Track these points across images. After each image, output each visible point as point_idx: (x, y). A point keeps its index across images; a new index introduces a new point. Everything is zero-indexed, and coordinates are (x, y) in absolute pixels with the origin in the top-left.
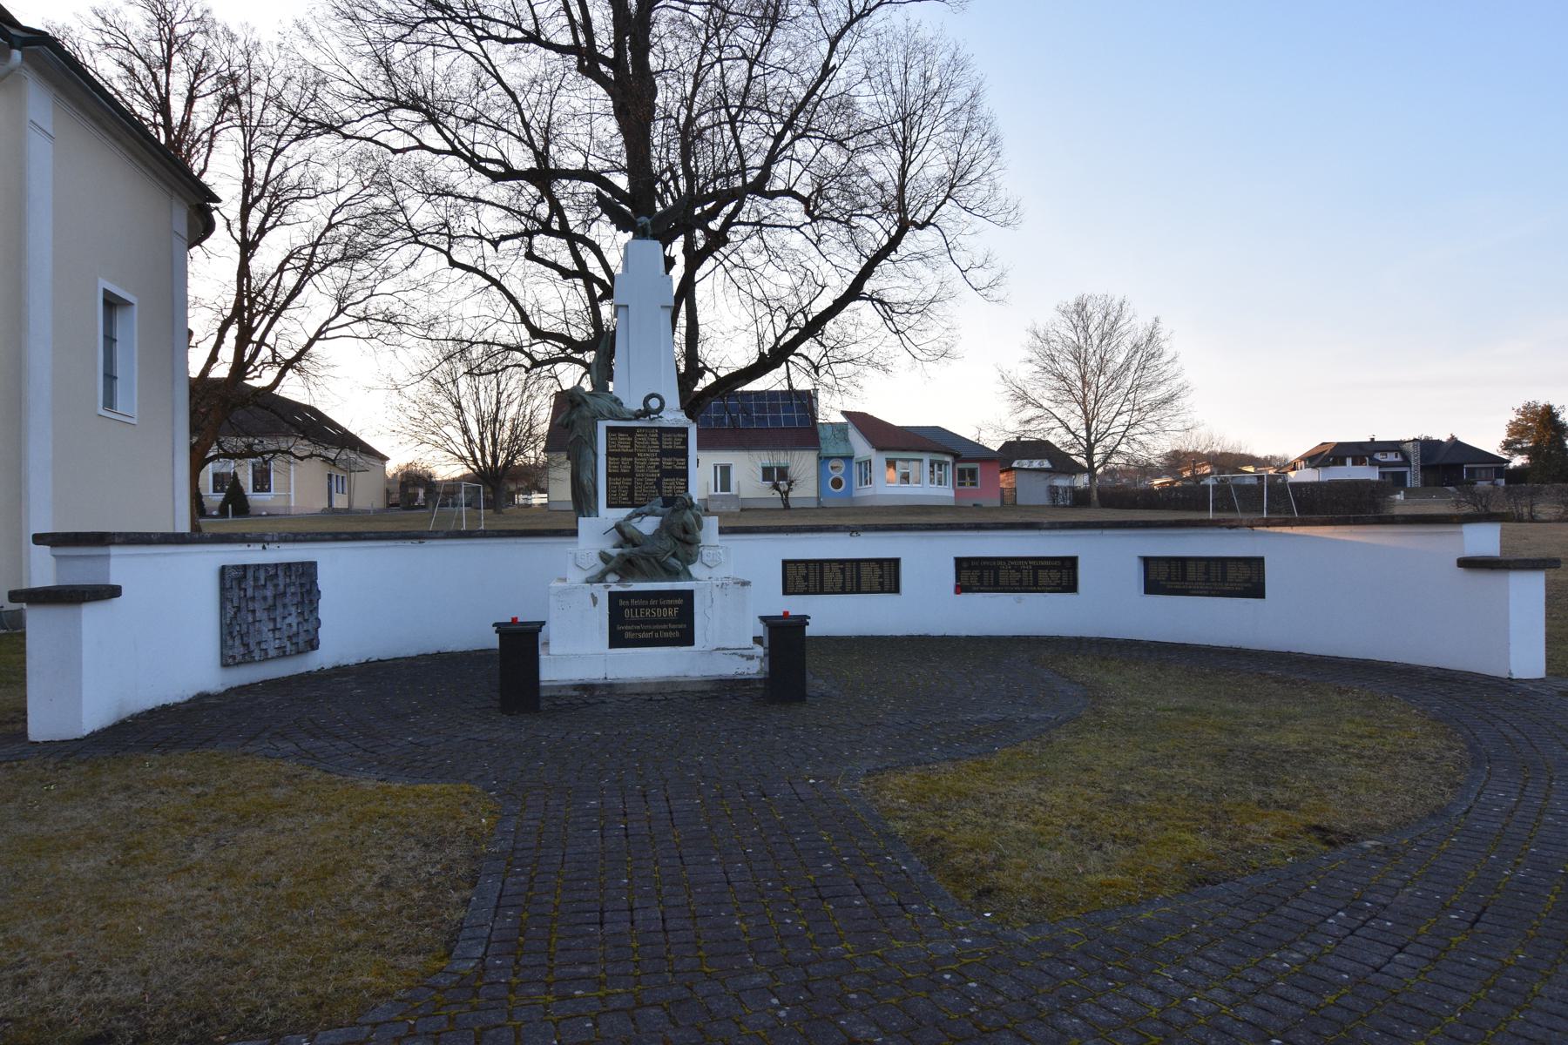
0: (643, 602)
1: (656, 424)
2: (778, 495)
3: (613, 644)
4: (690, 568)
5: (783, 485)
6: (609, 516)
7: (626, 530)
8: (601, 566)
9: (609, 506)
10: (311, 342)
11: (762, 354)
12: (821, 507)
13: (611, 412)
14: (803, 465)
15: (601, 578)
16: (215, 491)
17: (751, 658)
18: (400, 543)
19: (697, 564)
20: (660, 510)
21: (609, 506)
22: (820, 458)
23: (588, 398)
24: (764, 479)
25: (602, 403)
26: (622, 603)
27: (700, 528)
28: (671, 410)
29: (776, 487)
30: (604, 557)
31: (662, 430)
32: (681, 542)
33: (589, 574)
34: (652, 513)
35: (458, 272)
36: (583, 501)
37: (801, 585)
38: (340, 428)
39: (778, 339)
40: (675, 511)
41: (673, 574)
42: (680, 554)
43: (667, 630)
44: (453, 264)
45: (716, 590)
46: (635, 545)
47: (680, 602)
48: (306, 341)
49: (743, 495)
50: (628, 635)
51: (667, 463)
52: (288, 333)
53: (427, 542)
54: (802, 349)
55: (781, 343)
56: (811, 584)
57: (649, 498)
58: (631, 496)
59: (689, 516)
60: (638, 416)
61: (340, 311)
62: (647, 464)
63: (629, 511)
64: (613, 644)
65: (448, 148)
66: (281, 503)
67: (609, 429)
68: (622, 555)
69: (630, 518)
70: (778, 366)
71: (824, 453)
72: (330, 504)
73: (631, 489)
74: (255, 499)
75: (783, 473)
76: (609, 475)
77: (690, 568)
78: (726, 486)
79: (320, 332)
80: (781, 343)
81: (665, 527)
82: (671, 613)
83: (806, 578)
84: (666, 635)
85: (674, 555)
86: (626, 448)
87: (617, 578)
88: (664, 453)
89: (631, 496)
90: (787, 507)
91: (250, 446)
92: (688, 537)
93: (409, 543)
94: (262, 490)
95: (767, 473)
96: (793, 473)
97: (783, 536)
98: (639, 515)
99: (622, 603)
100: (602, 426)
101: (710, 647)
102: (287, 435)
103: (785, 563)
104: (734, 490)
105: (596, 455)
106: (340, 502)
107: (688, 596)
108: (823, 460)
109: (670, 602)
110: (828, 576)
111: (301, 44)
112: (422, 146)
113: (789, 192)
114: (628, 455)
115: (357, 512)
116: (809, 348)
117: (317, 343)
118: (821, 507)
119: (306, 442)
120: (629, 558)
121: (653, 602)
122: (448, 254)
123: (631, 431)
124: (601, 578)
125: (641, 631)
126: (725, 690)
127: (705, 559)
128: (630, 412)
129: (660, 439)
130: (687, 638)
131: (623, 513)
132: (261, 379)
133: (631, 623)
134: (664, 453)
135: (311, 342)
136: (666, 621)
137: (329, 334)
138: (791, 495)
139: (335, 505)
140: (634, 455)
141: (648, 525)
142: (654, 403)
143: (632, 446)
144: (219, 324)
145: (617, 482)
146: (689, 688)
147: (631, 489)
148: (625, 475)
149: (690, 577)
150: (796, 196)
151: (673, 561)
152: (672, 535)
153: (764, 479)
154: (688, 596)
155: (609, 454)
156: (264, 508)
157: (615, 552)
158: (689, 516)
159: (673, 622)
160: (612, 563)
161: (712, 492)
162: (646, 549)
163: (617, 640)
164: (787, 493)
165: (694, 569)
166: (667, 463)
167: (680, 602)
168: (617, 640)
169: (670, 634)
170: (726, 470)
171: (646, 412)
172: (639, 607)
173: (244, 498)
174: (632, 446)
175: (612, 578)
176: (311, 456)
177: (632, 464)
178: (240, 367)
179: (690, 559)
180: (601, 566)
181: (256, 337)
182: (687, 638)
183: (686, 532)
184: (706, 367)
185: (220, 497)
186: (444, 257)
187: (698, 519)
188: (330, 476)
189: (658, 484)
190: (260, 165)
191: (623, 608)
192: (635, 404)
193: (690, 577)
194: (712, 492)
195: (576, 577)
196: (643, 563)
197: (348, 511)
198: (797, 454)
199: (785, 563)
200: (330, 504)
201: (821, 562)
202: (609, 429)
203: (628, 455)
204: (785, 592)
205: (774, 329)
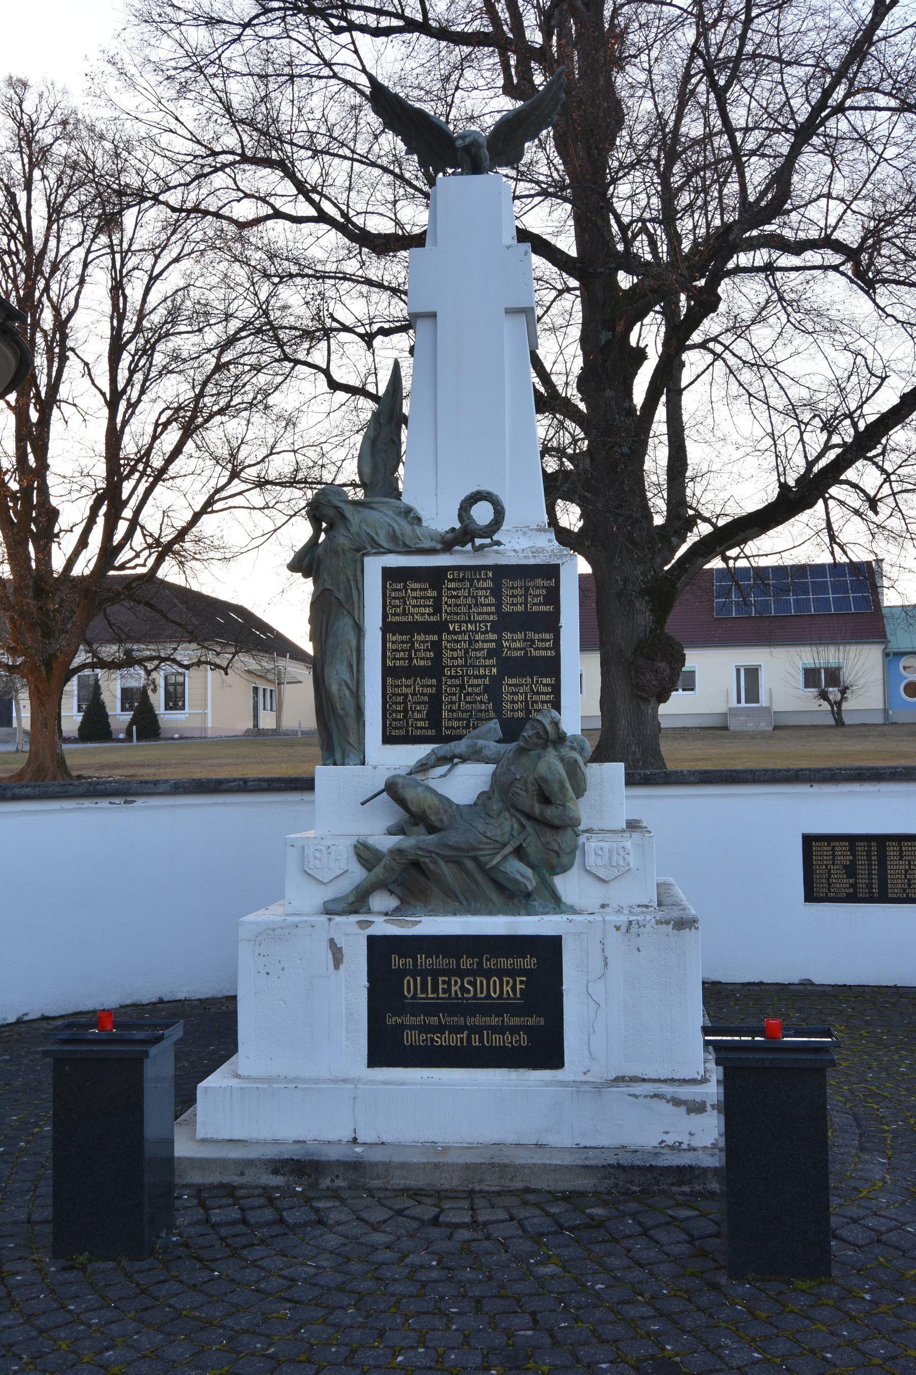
0: (442, 962)
1: (490, 559)
2: (826, 706)
3: (376, 1058)
4: (560, 882)
5: (834, 693)
6: (390, 760)
7: (410, 795)
8: (358, 874)
9: (388, 739)
10: (196, 517)
11: (783, 486)
12: (889, 723)
13: (394, 537)
14: (862, 664)
15: (356, 904)
16: (123, 709)
17: (697, 1108)
18: (87, 803)
19: (574, 873)
20: (491, 747)
21: (388, 739)
22: (886, 655)
23: (348, 511)
24: (807, 685)
25: (381, 519)
26: (397, 962)
27: (580, 790)
28: (524, 530)
29: (824, 696)
30: (365, 854)
31: (503, 572)
32: (537, 827)
33: (330, 893)
34: (475, 756)
35: (341, 396)
36: (336, 733)
37: (842, 884)
38: (270, 629)
39: (810, 465)
40: (522, 751)
41: (516, 898)
42: (532, 850)
43: (500, 1030)
44: (334, 385)
45: (615, 940)
46: (432, 829)
47: (529, 963)
48: (189, 516)
49: (777, 707)
50: (411, 1038)
51: (514, 644)
52: (165, 508)
53: (140, 802)
54: (850, 474)
55: (815, 469)
56: (862, 881)
57: (472, 722)
58: (434, 718)
59: (551, 763)
60: (449, 543)
61: (235, 475)
62: (473, 644)
63: (422, 751)
64: (376, 1058)
65: (313, 212)
66: (197, 723)
67: (389, 574)
68: (398, 852)
69: (423, 767)
70: (811, 505)
71: (893, 646)
72: (256, 725)
73: (435, 703)
74: (167, 718)
75: (834, 676)
76: (387, 672)
77: (560, 882)
78: (753, 694)
79: (210, 502)
80: (815, 469)
81: (501, 790)
82: (509, 989)
83: (850, 871)
84: (497, 1040)
85: (519, 853)
86: (422, 614)
87: (391, 902)
88: (506, 622)
89: (434, 718)
90: (840, 723)
91: (128, 653)
92: (550, 813)
93: (104, 803)
94: (175, 707)
95: (811, 677)
96: (847, 676)
97: (804, 789)
98: (446, 759)
99: (397, 962)
100: (373, 568)
101: (600, 1073)
102: (171, 638)
103: (809, 840)
104: (764, 701)
105: (359, 630)
106: (267, 721)
107: (549, 949)
108: (891, 657)
109: (505, 963)
110: (895, 867)
111: (113, 85)
112: (278, 214)
113: (827, 242)
114: (426, 628)
115: (286, 733)
116: (864, 474)
117: (205, 518)
118: (889, 723)
119: (194, 646)
120: (418, 859)
121: (467, 963)
122: (326, 372)
123: (436, 576)
124: (356, 904)
125: (440, 1029)
126: (636, 1185)
127: (591, 860)
128: (433, 536)
129: (496, 592)
130: (545, 1050)
131: (411, 755)
132: (135, 559)
133: (440, 1005)
134: (506, 622)
135: (196, 517)
136: (499, 1008)
137: (217, 507)
138: (845, 706)
139: (262, 725)
140: (440, 628)
141: (465, 783)
142: (482, 513)
143: (437, 609)
144: (91, 502)
145: (406, 685)
146: (540, 1184)
147: (435, 703)
148: (423, 672)
149: (556, 904)
150: (838, 247)
151: (516, 868)
152: (513, 807)
153: (807, 685)
154: (549, 949)
155: (387, 628)
156: (176, 730)
157: (386, 843)
158: (551, 763)
159: (515, 1010)
160: (378, 870)
161: (733, 703)
162: (454, 838)
163: (385, 1049)
164: (839, 704)
165: (568, 885)
166: (514, 644)
167: (529, 963)
168: (385, 1049)
169: (509, 1040)
170: (752, 673)
171: (465, 534)
172: (435, 973)
173: (155, 717)
174: (437, 609)
175: (382, 901)
176: (199, 663)
177: (436, 647)
178: (109, 552)
179: (554, 862)
180: (358, 874)
181: (128, 513)
182: (545, 1050)
183: (546, 800)
184: (699, 515)
185: (128, 716)
186: (321, 376)
187: (573, 770)
188: (256, 690)
189: (493, 690)
190: (134, 291)
191: (402, 973)
192: (441, 518)
193: (556, 904)
194: (733, 703)
195: (304, 898)
196: (447, 871)
197: (276, 732)
198: (853, 650)
199: (809, 840)
200: (256, 725)
201: (882, 840)
202: (389, 574)
203: (426, 628)
204: (811, 896)
205: (807, 447)
